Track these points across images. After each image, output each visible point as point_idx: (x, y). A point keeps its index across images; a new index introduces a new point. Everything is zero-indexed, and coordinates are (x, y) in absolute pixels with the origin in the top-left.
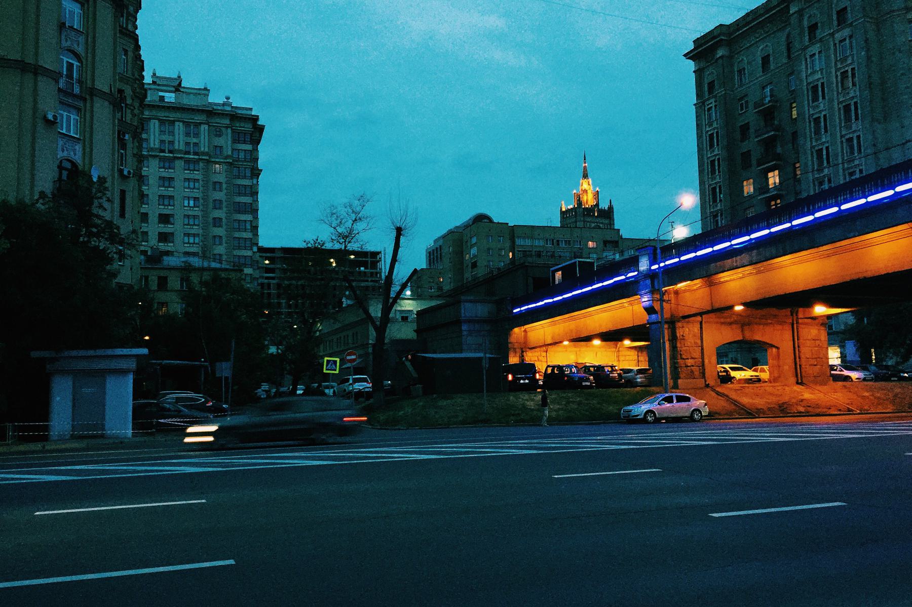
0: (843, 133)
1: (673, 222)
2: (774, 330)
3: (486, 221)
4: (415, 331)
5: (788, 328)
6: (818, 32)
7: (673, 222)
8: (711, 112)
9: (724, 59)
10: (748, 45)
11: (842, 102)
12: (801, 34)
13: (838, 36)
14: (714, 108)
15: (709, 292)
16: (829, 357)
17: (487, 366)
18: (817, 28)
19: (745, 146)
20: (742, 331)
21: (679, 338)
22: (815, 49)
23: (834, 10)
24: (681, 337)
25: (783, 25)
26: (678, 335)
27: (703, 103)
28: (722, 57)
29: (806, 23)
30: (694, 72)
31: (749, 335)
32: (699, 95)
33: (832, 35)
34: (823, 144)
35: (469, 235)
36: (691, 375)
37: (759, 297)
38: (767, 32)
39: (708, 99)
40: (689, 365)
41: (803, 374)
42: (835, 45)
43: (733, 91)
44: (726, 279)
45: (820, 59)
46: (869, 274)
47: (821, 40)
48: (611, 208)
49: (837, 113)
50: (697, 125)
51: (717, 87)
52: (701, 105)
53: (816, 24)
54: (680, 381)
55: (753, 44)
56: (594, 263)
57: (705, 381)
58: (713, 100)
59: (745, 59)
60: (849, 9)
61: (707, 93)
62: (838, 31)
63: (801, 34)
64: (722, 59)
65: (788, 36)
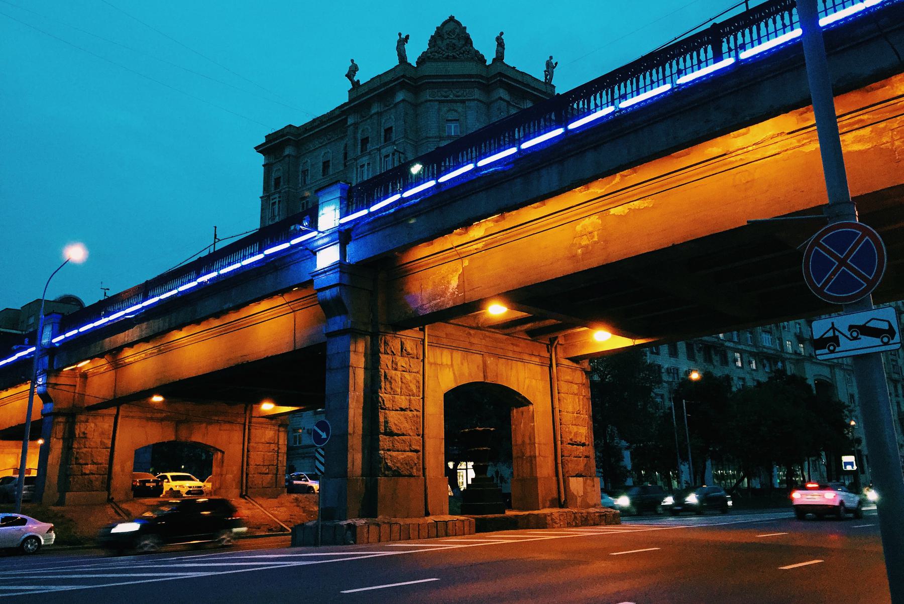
1: (108, 289)
2: (220, 430)
5: (238, 428)
6: (369, 146)
7: (108, 289)
8: (274, 207)
10: (313, 148)
12: (355, 145)
13: (383, 151)
14: (277, 203)
15: (114, 377)
16: (36, 471)
18: (368, 142)
20: (177, 431)
21: (77, 436)
22: (365, 160)
23: (382, 128)
24: (82, 435)
25: (342, 135)
26: (77, 432)
27: (269, 197)
28: (288, 156)
29: (359, 136)
30: (263, 166)
31: (184, 435)
32: (266, 189)
33: (379, 150)
36: (89, 487)
37: (158, 384)
38: (330, 139)
39: (274, 194)
40: (87, 472)
41: (250, 484)
42: (381, 159)
43: (296, 190)
44: (130, 360)
45: (368, 170)
46: (252, 358)
47: (369, 153)
51: (282, 183)
52: (266, 199)
53: (367, 138)
54: (68, 495)
55: (317, 148)
57: (109, 494)
58: (277, 196)
59: (309, 161)
60: (394, 129)
61: (273, 189)
62: (384, 147)
63: (355, 145)
64: (289, 157)
65: (346, 144)
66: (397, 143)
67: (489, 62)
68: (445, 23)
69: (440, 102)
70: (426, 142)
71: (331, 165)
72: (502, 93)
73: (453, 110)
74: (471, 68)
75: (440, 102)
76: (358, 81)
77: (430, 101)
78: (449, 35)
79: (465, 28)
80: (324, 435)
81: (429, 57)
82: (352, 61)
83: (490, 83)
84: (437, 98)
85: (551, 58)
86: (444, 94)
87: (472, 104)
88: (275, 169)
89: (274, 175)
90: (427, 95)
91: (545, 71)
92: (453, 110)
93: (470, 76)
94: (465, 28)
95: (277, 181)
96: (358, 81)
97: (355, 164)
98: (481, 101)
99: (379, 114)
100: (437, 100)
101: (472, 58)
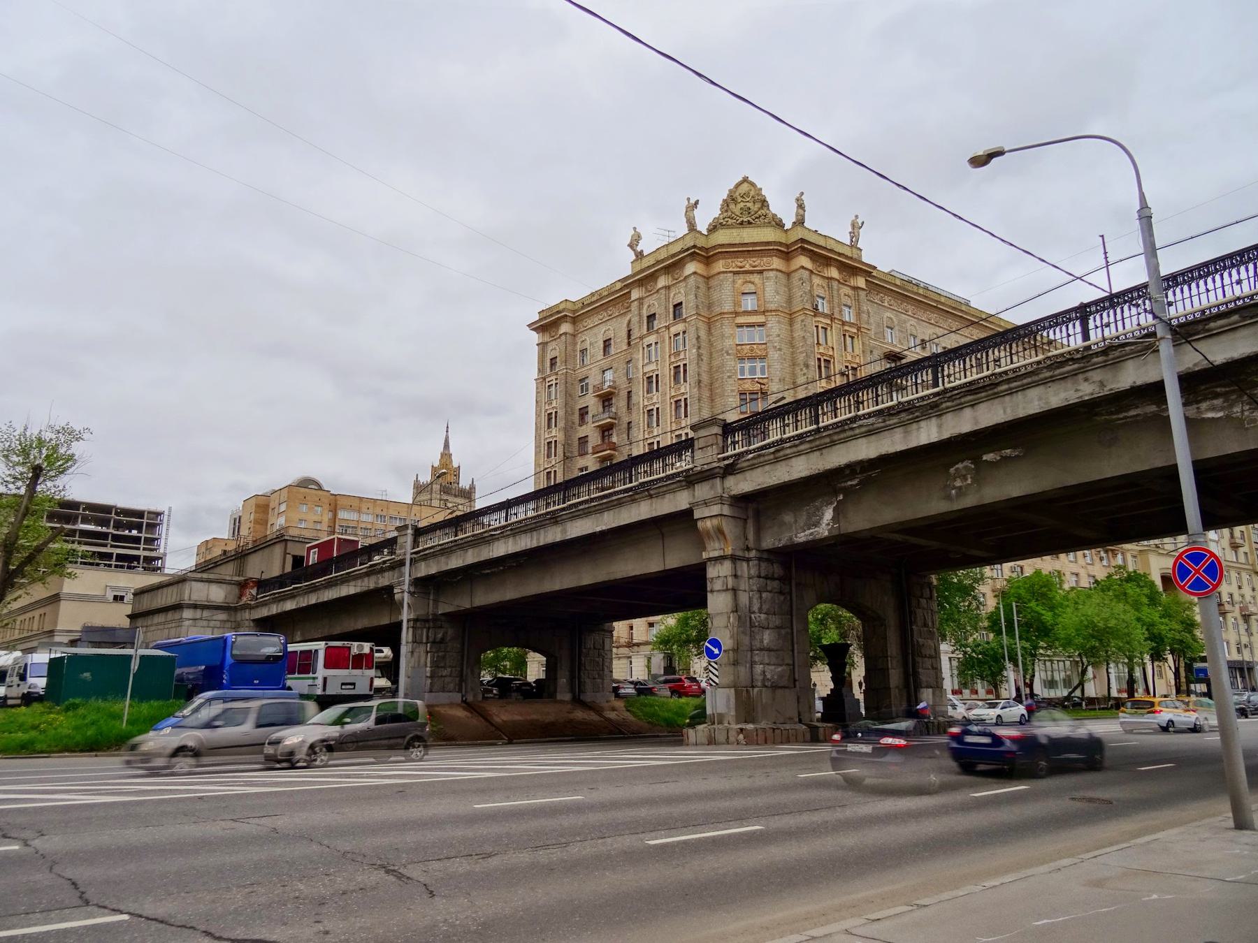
3: (313, 487)
4: (128, 616)
12: (640, 322)
17: (136, 667)
29: (645, 313)
32: (541, 370)
35: (277, 502)
45: (656, 349)
48: (472, 487)
56: (357, 542)
61: (548, 369)
67: (788, 226)
69: (735, 273)
72: (804, 261)
73: (750, 282)
75: (735, 273)
77: (724, 272)
79: (761, 189)
80: (716, 651)
81: (721, 224)
82: (635, 228)
84: (731, 269)
85: (857, 217)
86: (740, 264)
87: (772, 274)
90: (719, 266)
91: (850, 233)
92: (750, 282)
93: (768, 243)
94: (761, 189)
95: (553, 361)
96: (642, 251)
98: (780, 271)
99: (668, 288)
100: (731, 272)
101: (769, 223)
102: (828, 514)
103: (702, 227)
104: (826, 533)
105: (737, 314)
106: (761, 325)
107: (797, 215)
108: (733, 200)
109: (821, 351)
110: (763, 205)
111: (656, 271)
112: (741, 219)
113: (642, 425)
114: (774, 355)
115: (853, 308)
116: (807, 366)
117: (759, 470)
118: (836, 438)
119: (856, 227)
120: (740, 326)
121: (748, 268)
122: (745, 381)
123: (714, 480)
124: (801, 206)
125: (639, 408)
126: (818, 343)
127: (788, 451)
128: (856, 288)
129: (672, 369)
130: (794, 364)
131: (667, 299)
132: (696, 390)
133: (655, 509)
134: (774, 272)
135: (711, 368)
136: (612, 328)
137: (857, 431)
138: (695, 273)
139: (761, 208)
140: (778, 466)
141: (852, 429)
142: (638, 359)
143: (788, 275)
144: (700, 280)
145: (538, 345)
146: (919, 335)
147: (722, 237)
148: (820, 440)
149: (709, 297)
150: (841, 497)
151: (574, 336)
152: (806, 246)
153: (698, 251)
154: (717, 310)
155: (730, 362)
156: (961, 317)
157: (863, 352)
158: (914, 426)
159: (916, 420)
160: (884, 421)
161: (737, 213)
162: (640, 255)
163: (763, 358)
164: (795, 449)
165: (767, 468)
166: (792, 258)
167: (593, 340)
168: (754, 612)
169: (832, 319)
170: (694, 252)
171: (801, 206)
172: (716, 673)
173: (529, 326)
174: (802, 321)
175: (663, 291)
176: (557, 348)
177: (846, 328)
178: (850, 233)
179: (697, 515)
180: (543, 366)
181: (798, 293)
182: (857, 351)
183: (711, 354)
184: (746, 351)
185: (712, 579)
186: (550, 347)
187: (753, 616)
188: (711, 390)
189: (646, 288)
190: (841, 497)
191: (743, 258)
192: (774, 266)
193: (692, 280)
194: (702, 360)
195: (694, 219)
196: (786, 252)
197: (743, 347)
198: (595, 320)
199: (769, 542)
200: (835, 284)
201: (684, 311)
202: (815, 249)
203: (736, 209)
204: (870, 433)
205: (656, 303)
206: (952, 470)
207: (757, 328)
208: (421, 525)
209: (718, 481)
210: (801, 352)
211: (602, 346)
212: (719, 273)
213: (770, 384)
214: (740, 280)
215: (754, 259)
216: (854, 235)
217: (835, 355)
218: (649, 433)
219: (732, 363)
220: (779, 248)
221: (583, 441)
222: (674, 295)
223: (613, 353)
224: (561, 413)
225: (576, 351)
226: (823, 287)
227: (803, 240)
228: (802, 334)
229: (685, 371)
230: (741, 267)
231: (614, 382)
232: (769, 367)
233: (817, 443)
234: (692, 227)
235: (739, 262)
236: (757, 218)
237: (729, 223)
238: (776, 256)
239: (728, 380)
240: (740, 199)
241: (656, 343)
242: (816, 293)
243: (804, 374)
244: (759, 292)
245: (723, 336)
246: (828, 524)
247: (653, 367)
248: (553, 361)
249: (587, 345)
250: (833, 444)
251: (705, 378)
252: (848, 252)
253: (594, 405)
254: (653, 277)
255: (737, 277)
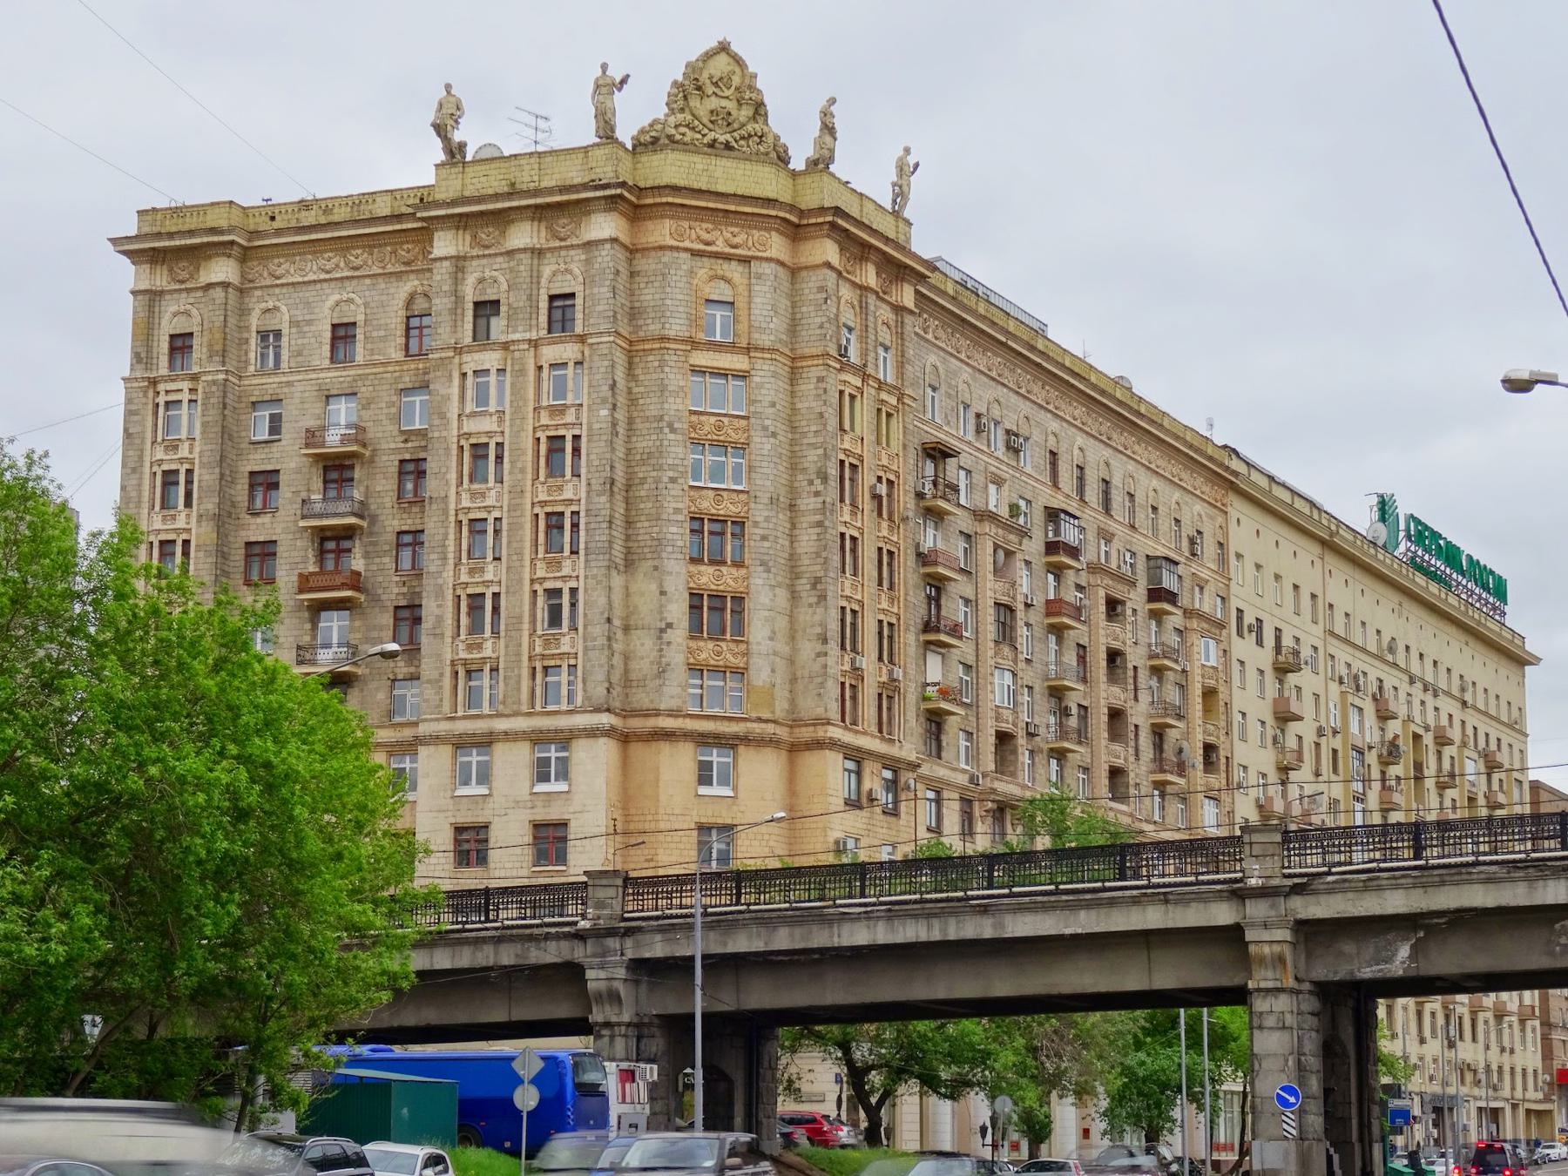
0: (540, 573)
9: (230, 290)
11: (543, 503)
12: (456, 310)
19: (259, 529)
29: (470, 294)
32: (141, 357)
34: (487, 583)
45: (501, 385)
49: (528, 526)
50: (128, 434)
59: (284, 309)
61: (164, 360)
66: (590, 341)
67: (798, 164)
68: (708, 56)
70: (661, 348)
71: (360, 337)
72: (829, 250)
73: (723, 278)
74: (763, 181)
76: (462, 146)
77: (672, 248)
78: (718, 87)
79: (755, 76)
80: (1292, 1100)
81: (670, 137)
82: (448, 87)
83: (805, 222)
84: (687, 244)
85: (907, 151)
86: (706, 236)
87: (767, 269)
88: (173, 308)
89: (168, 325)
90: (661, 231)
91: (894, 185)
92: (723, 278)
93: (770, 202)
94: (755, 76)
97: (457, 360)
99: (538, 253)
100: (686, 250)
101: (767, 154)
102: (1404, 951)
103: (625, 133)
104: (1401, 972)
105: (694, 344)
106: (743, 376)
107: (819, 143)
108: (699, 88)
109: (847, 445)
110: (756, 112)
111: (511, 209)
112: (711, 135)
113: (451, 549)
114: (762, 446)
115: (892, 351)
116: (825, 478)
117: (1339, 896)
118: (1447, 878)
119: (905, 170)
120: (698, 371)
121: (720, 247)
122: (704, 492)
123: (1277, 899)
124: (829, 129)
125: (445, 512)
126: (842, 429)
127: (1384, 882)
128: (899, 309)
129: (543, 440)
130: (794, 467)
131: (535, 278)
132: (603, 499)
133: (1173, 919)
134: (773, 265)
135: (629, 451)
136: (359, 301)
137: (1475, 876)
138: (614, 240)
139: (754, 119)
140: (1367, 895)
141: (1470, 873)
142: (448, 398)
143: (794, 271)
144: (622, 255)
145: (133, 292)
146: (973, 404)
147: (669, 168)
148: (1427, 877)
149: (631, 293)
150: (1421, 934)
151: (241, 291)
152: (840, 222)
153: (626, 194)
154: (653, 328)
155: (677, 451)
156: (1038, 365)
157: (905, 447)
158: (1541, 883)
159: (1544, 878)
160: (1509, 872)
161: (705, 121)
162: (455, 152)
163: (741, 448)
164: (1394, 882)
165: (1350, 895)
166: (806, 239)
167: (300, 315)
168: (1304, 1054)
169: (865, 377)
170: (621, 196)
171: (829, 129)
172: (1285, 1126)
173: (114, 241)
174: (820, 379)
175: (525, 258)
176: (194, 312)
177: (884, 396)
178: (894, 185)
179: (1250, 935)
180: (149, 349)
181: (813, 319)
182: (896, 446)
183: (630, 421)
184: (707, 428)
185: (1261, 1013)
186: (170, 307)
187: (1303, 1058)
188: (627, 501)
189: (474, 237)
190: (1421, 934)
191: (714, 223)
192: (773, 253)
193: (606, 256)
194: (617, 433)
195: (614, 114)
196: (797, 228)
197: (703, 418)
198: (311, 269)
199: (1322, 972)
200: (872, 299)
201: (579, 316)
202: (853, 229)
203: (703, 107)
204: (1490, 880)
205: (502, 279)
206: (1557, 926)
207: (732, 382)
208: (633, 874)
209: (1282, 899)
210: (813, 446)
211: (328, 335)
212: (661, 248)
213: (752, 505)
214: (704, 268)
215: (736, 230)
216: (901, 194)
217: (865, 455)
218: (471, 572)
219: (680, 450)
220: (788, 216)
221: (262, 552)
222: (554, 274)
223: (359, 359)
224: (204, 477)
225: (248, 328)
226: (853, 308)
227: (837, 211)
228: (817, 406)
229: (576, 451)
230: (707, 244)
231: (360, 429)
232: (751, 468)
233: (1424, 880)
234: (607, 132)
235: (702, 230)
236: (743, 138)
237: (687, 139)
238: (777, 230)
239: (670, 486)
240: (710, 89)
241: (501, 371)
242: (843, 320)
243: (817, 494)
244: (741, 304)
245: (663, 389)
246: (1404, 962)
247: (488, 424)
248: (180, 344)
249: (282, 321)
250: (1443, 883)
251: (620, 475)
252: (886, 225)
253: (298, 471)
254: (501, 219)
255: (699, 262)
